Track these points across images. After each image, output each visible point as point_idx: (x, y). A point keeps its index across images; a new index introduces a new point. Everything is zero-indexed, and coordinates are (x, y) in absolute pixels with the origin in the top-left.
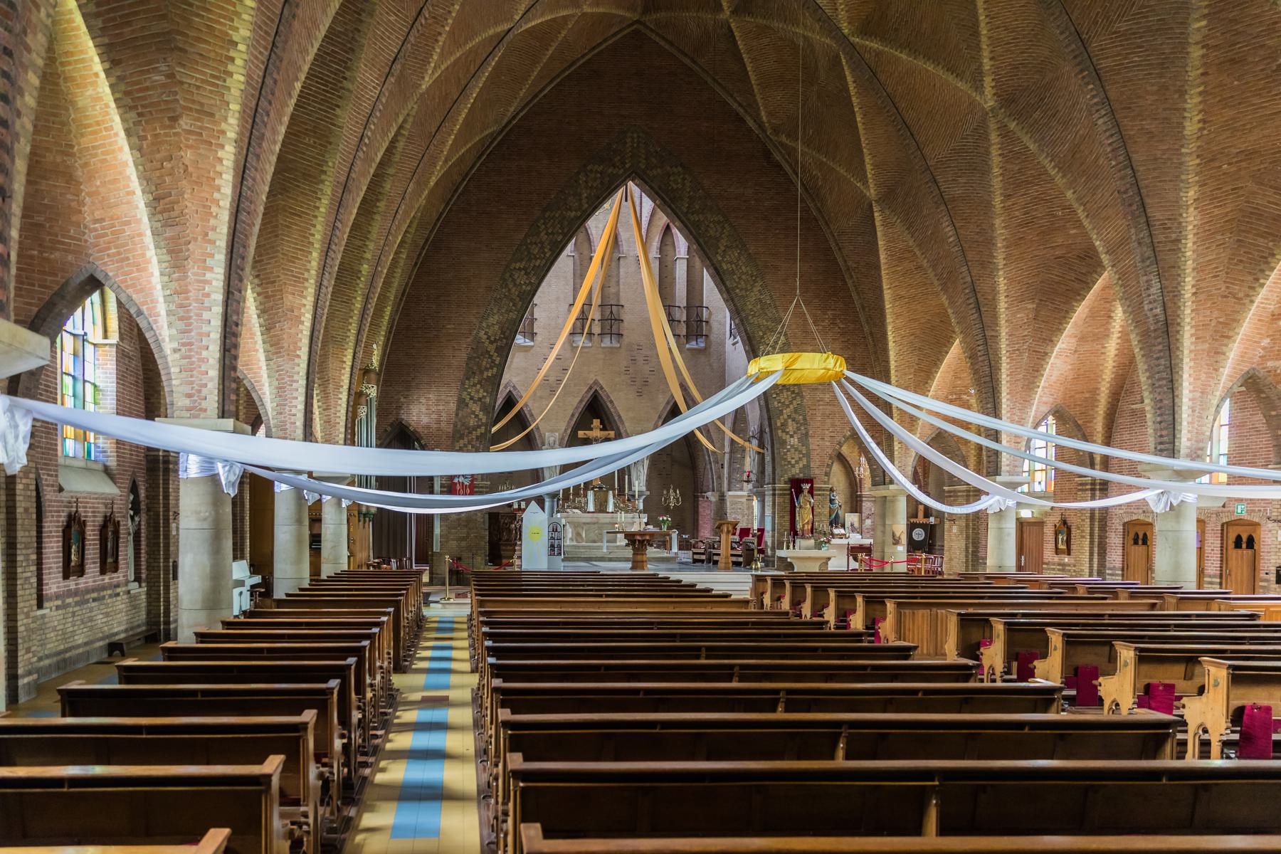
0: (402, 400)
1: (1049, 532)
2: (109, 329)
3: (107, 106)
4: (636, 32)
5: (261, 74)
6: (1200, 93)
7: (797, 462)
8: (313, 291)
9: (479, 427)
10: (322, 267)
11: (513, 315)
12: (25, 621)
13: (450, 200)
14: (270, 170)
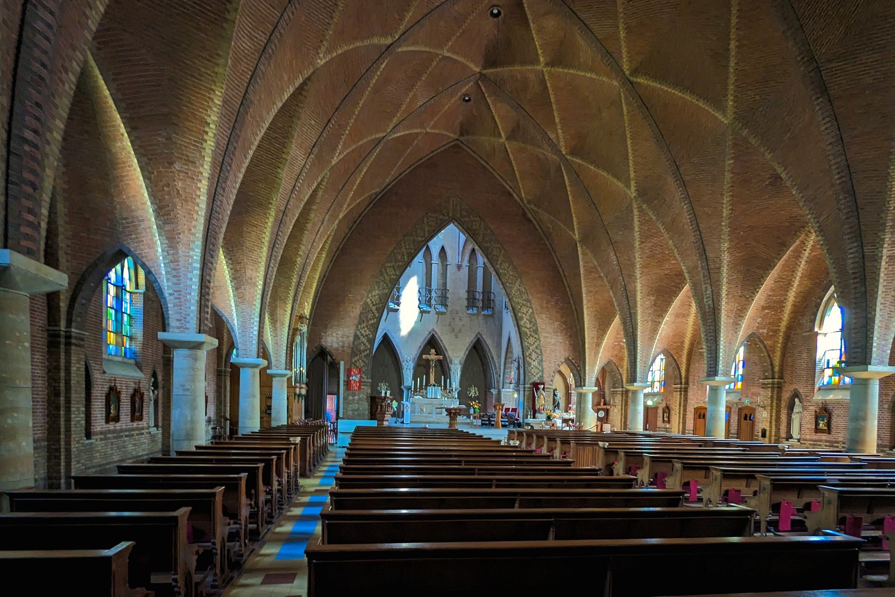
0: (323, 334)
1: (660, 412)
2: (140, 284)
3: (129, 153)
4: (456, 145)
5: (226, 143)
6: (731, 196)
7: (537, 374)
8: (264, 269)
9: (366, 350)
10: (269, 256)
11: (386, 291)
12: (76, 445)
13: (352, 227)
14: (233, 198)
